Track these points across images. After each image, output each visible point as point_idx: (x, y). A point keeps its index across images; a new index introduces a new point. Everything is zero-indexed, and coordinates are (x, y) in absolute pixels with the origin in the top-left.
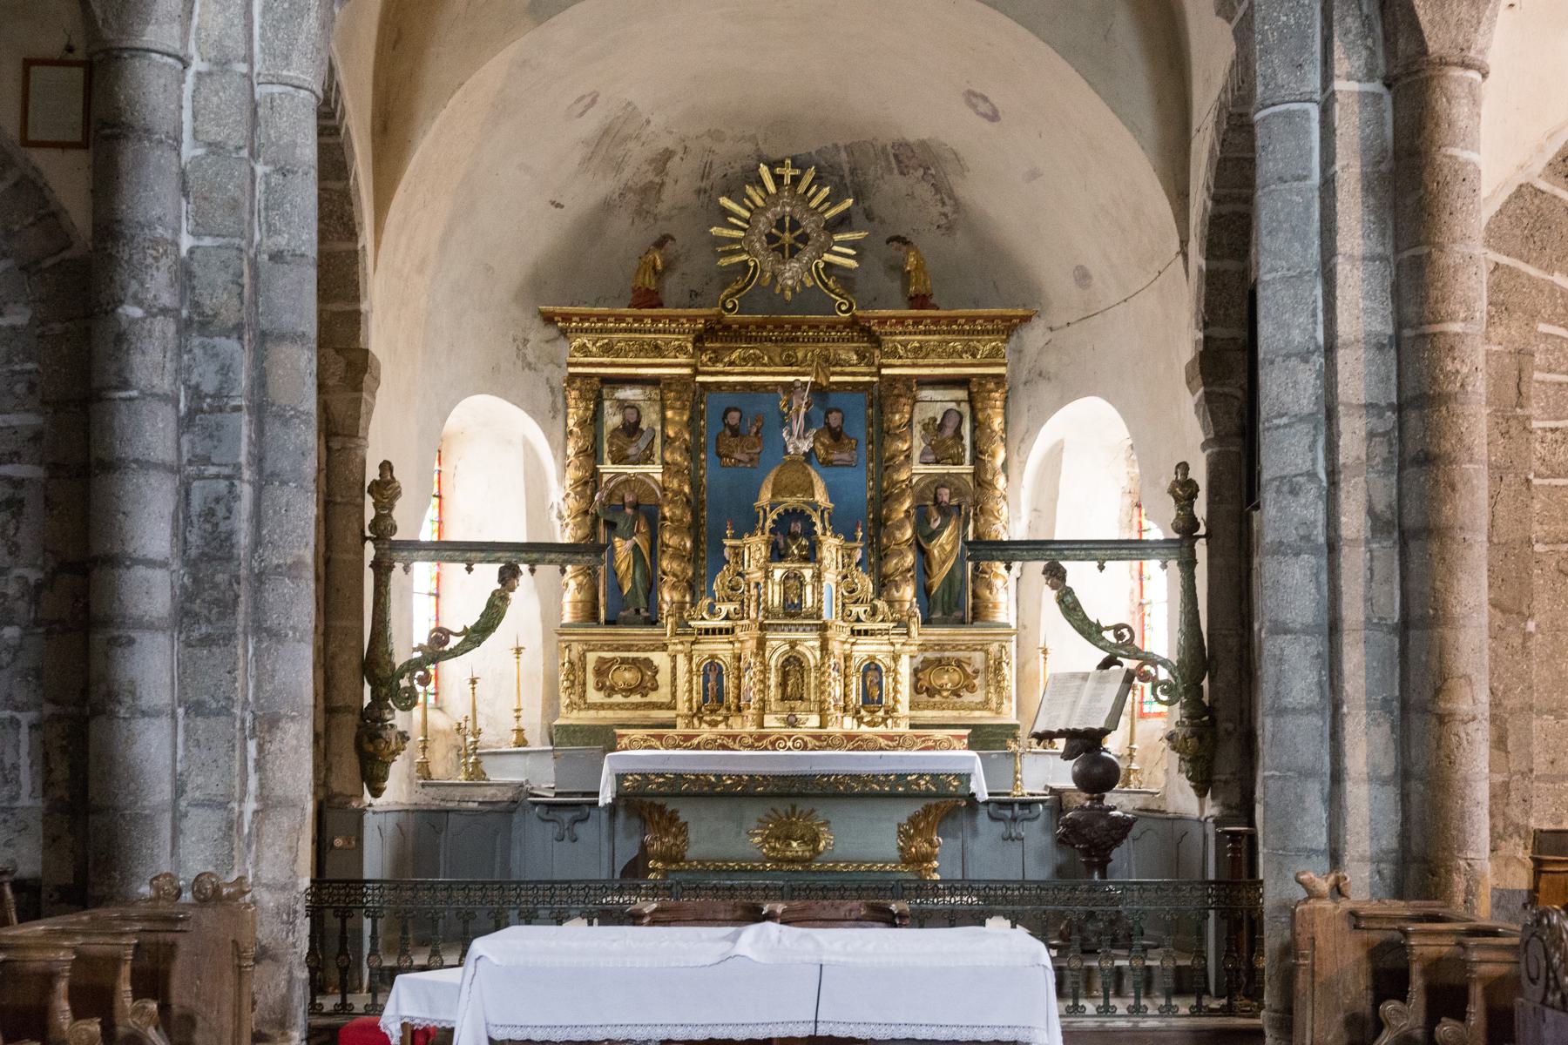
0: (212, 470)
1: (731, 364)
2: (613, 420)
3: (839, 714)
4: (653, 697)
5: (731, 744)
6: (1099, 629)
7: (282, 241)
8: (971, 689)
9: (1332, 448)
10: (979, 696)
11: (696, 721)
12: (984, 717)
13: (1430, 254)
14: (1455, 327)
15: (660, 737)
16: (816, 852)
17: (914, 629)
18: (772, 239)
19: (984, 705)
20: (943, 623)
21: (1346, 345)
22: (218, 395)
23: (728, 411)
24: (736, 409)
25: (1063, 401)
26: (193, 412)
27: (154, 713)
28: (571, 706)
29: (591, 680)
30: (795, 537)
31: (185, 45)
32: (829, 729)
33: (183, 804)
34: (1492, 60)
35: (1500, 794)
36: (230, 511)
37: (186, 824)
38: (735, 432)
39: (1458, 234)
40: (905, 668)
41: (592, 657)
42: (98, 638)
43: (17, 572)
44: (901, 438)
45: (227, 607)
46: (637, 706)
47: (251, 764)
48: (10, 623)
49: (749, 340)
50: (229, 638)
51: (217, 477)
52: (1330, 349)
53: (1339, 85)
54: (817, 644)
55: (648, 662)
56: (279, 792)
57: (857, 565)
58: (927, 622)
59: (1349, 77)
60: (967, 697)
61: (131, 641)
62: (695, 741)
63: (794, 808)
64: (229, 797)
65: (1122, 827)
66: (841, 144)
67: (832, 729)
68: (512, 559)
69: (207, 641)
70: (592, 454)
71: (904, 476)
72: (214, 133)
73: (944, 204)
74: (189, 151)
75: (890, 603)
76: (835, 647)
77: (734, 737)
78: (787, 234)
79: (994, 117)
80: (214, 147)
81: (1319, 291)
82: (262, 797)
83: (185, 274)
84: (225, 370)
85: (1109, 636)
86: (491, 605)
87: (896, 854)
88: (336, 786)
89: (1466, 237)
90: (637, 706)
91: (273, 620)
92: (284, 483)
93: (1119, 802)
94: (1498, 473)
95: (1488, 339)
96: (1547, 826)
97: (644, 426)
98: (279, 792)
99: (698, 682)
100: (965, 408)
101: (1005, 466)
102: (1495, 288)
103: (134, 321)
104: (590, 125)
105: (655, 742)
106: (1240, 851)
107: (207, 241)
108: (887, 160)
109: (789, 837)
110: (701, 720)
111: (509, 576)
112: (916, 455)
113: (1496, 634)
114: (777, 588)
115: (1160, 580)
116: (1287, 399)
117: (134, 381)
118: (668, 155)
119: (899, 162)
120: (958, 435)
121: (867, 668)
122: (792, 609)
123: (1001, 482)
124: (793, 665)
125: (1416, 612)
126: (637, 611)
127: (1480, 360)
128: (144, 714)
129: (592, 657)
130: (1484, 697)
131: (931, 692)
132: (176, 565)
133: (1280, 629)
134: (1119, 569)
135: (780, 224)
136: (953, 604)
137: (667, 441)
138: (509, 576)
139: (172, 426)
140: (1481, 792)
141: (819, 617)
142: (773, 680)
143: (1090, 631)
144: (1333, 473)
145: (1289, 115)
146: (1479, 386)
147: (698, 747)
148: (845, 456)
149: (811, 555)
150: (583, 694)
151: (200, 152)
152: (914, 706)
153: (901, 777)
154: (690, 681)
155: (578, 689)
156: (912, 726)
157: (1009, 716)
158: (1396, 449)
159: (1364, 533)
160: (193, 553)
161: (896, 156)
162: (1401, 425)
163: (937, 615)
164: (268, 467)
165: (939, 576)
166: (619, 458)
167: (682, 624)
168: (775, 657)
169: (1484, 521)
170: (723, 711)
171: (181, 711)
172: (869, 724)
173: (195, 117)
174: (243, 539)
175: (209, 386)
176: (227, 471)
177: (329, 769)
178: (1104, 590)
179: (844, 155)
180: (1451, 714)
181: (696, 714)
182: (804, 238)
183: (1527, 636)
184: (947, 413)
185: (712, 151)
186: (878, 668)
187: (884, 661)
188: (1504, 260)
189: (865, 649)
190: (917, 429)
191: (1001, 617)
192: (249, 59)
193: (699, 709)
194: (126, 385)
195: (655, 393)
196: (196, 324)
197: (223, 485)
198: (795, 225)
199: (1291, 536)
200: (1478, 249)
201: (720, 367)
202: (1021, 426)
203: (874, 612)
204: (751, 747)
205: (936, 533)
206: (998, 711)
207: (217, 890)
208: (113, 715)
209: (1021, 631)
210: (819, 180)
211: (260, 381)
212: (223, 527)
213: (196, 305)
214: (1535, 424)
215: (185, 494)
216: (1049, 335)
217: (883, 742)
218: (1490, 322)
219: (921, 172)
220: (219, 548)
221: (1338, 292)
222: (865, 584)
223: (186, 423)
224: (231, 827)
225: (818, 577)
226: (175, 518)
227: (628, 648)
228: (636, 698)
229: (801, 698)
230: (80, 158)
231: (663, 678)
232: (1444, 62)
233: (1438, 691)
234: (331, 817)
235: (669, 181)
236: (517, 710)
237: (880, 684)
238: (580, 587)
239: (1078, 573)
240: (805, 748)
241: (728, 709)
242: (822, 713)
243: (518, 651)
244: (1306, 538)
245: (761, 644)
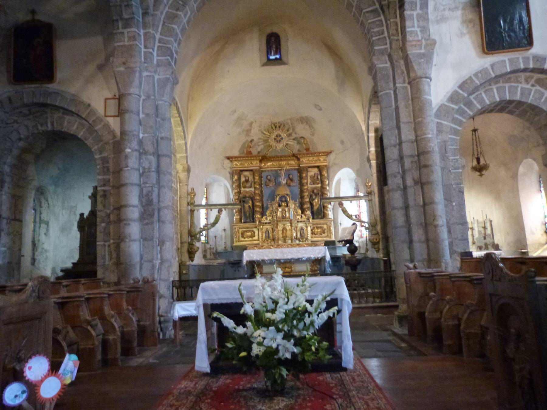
0: (148, 185)
2: (243, 179)
4: (254, 238)
6: (352, 216)
7: (163, 135)
8: (324, 233)
9: (403, 166)
10: (326, 234)
12: (328, 239)
13: (422, 120)
14: (430, 136)
16: (292, 270)
17: (311, 220)
19: (327, 236)
20: (317, 218)
21: (405, 142)
22: (149, 168)
25: (339, 170)
26: (143, 173)
27: (135, 240)
28: (236, 241)
29: (240, 235)
31: (140, 92)
33: (142, 261)
34: (432, 76)
35: (451, 244)
36: (152, 194)
37: (144, 266)
38: (269, 180)
39: (428, 114)
42: (122, 224)
43: (105, 211)
44: (305, 179)
45: (152, 216)
46: (251, 241)
47: (158, 252)
48: (104, 222)
50: (152, 223)
51: (149, 187)
52: (400, 144)
53: (398, 85)
55: (253, 231)
56: (165, 258)
58: (313, 218)
59: (400, 83)
60: (323, 235)
61: (129, 224)
64: (153, 259)
65: (359, 261)
67: (294, 243)
68: (220, 207)
69: (147, 224)
70: (239, 186)
71: (306, 187)
72: (147, 111)
74: (142, 116)
75: (305, 215)
76: (293, 225)
79: (321, 109)
80: (147, 115)
81: (396, 132)
82: (161, 259)
83: (140, 142)
84: (150, 163)
85: (354, 217)
86: (216, 218)
88: (183, 260)
89: (430, 116)
90: (251, 241)
91: (163, 219)
92: (164, 188)
93: (358, 255)
94: (443, 169)
95: (437, 139)
96: (463, 251)
97: (250, 180)
98: (165, 258)
99: (264, 235)
101: (328, 184)
102: (438, 127)
103: (129, 153)
104: (236, 116)
106: (388, 263)
107: (146, 135)
111: (220, 211)
112: (309, 183)
113: (446, 206)
115: (363, 203)
116: (391, 156)
117: (129, 165)
122: (283, 218)
123: (328, 188)
125: (427, 201)
127: (436, 143)
128: (132, 241)
130: (445, 221)
132: (140, 207)
133: (394, 208)
134: (354, 202)
135: (277, 136)
136: (319, 213)
137: (255, 183)
138: (220, 211)
139: (138, 176)
140: (446, 243)
143: (350, 217)
144: (404, 172)
145: (386, 93)
146: (436, 149)
150: (239, 239)
151: (144, 116)
152: (312, 237)
157: (333, 238)
158: (418, 165)
159: (413, 184)
160: (144, 204)
162: (419, 160)
164: (161, 184)
165: (315, 208)
166: (245, 187)
167: (260, 222)
169: (440, 179)
171: (142, 240)
173: (143, 108)
174: (155, 200)
175: (147, 167)
176: (151, 185)
177: (182, 256)
178: (351, 207)
179: (289, 121)
180: (438, 225)
183: (453, 206)
184: (315, 174)
188: (439, 121)
189: (300, 225)
190: (309, 178)
191: (330, 217)
192: (154, 95)
194: (127, 166)
195: (251, 173)
196: (142, 153)
197: (150, 189)
198: (280, 136)
199: (395, 187)
200: (433, 118)
202: (331, 174)
203: (302, 217)
205: (314, 199)
206: (330, 237)
207: (148, 280)
208: (125, 242)
209: (335, 220)
211: (158, 166)
212: (151, 198)
213: (144, 149)
214: (450, 158)
215: (141, 191)
218: (437, 135)
220: (150, 202)
221: (402, 131)
223: (141, 175)
224: (153, 266)
225: (289, 210)
226: (139, 196)
227: (248, 228)
228: (250, 239)
230: (118, 119)
231: (256, 234)
232: (421, 78)
233: (434, 220)
234: (182, 267)
239: (347, 204)
242: (292, 240)
244: (399, 187)
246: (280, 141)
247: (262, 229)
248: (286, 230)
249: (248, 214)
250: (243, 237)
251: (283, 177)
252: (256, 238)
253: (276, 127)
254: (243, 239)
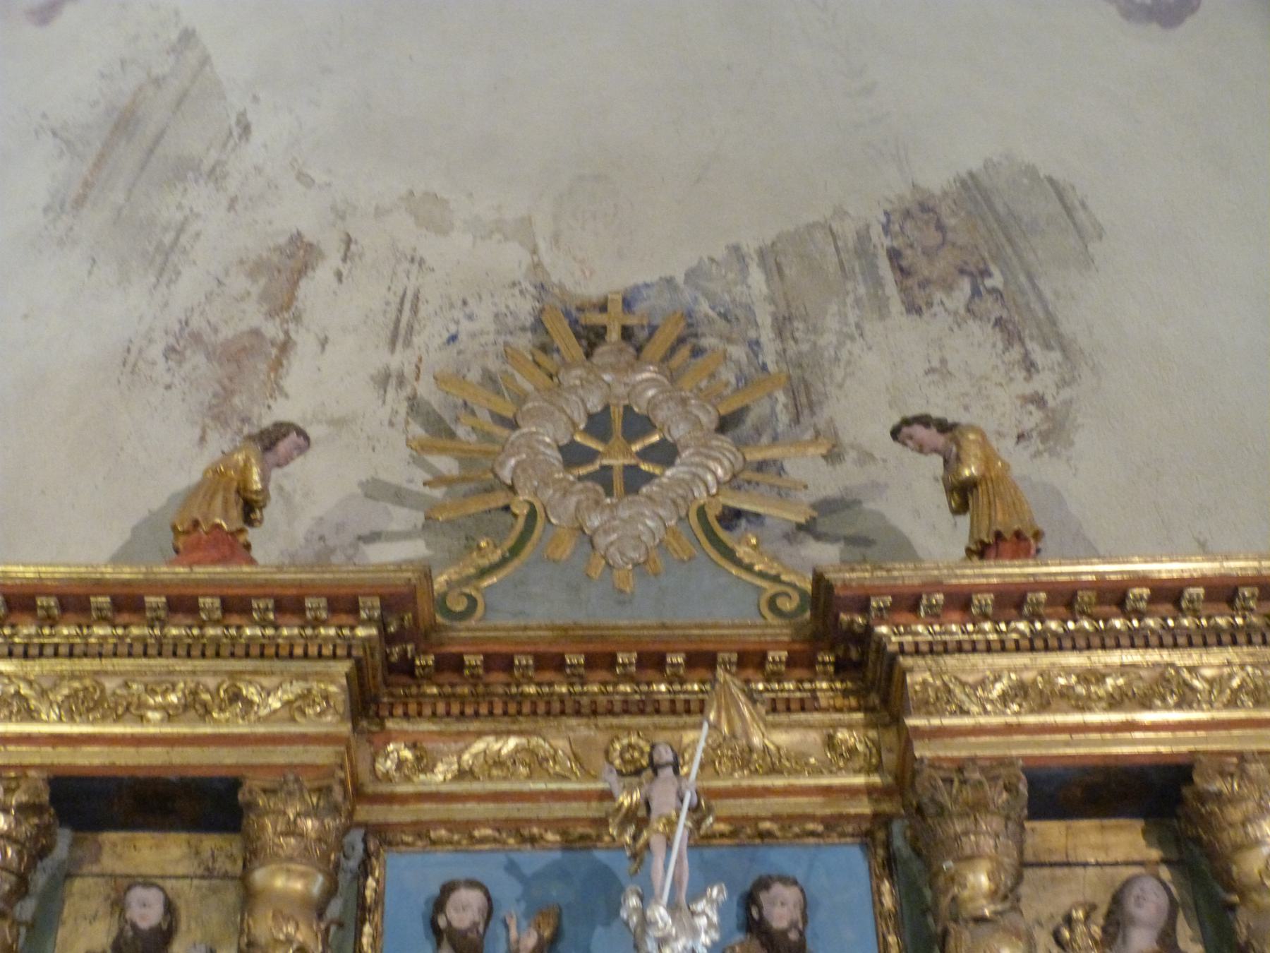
23: (448, 889)
24: (472, 884)
66: (750, 246)
73: (1030, 367)
108: (873, 267)
118: (299, 257)
119: (903, 272)
179: (757, 277)
182: (666, 453)
185: (417, 261)
210: (623, 826)
219: (965, 285)
235: (305, 341)
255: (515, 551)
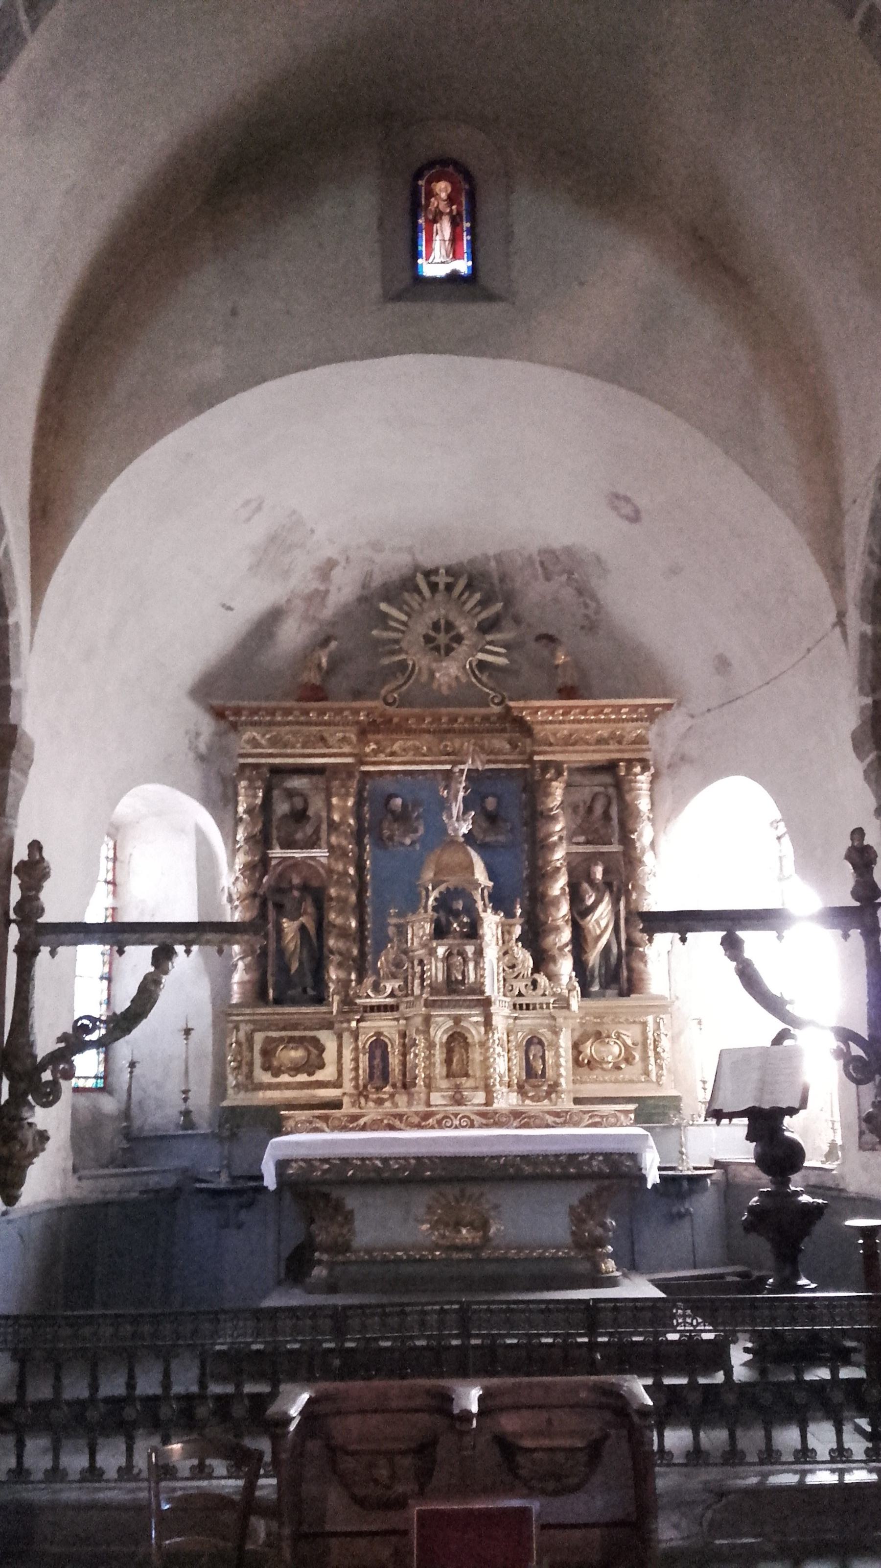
1: (393, 754)
3: (505, 1089)
5: (397, 1123)
11: (363, 1101)
15: (325, 1119)
16: (486, 1239)
18: (428, 639)
30: (457, 914)
32: (496, 1106)
40: (565, 1041)
41: (259, 1037)
49: (409, 731)
54: (480, 1019)
55: (316, 1042)
57: (517, 940)
58: (585, 993)
62: (362, 1122)
63: (462, 1191)
77: (400, 1116)
78: (442, 634)
87: (568, 1239)
100: (611, 791)
105: (319, 1124)
109: (457, 1225)
110: (367, 1098)
114: (440, 965)
120: (606, 816)
121: (530, 1043)
124: (457, 1040)
126: (305, 991)
129: (259, 1037)
131: (591, 1064)
135: (436, 626)
141: (483, 992)
142: (439, 1055)
147: (363, 1128)
148: (502, 838)
149: (473, 932)
150: (250, 1075)
153: (573, 1157)
154: (356, 1060)
155: (245, 1069)
156: (577, 1101)
161: (542, 563)
163: (596, 988)
168: (439, 1033)
170: (388, 1089)
172: (532, 1099)
181: (361, 1093)
182: (459, 639)
186: (541, 1043)
187: (546, 1035)
193: (365, 1087)
198: (450, 626)
201: (382, 757)
203: (535, 983)
204: (419, 1126)
216: (690, 722)
217: (550, 1119)
219: (564, 578)
222: (525, 958)
225: (479, 953)
228: (302, 1078)
229: (467, 1075)
231: (330, 1055)
235: (333, 589)
236: (186, 1092)
237: (543, 1058)
238: (247, 969)
240: (472, 1126)
241: (394, 1086)
243: (188, 1032)
245: (427, 1020)
246: (449, 650)
247: (356, 1034)
248: (466, 1045)
249: (295, 966)
250: (266, 1068)
251: (457, 808)
252: (327, 1074)
253: (433, 587)
254: (266, 1078)
255: (410, 677)
